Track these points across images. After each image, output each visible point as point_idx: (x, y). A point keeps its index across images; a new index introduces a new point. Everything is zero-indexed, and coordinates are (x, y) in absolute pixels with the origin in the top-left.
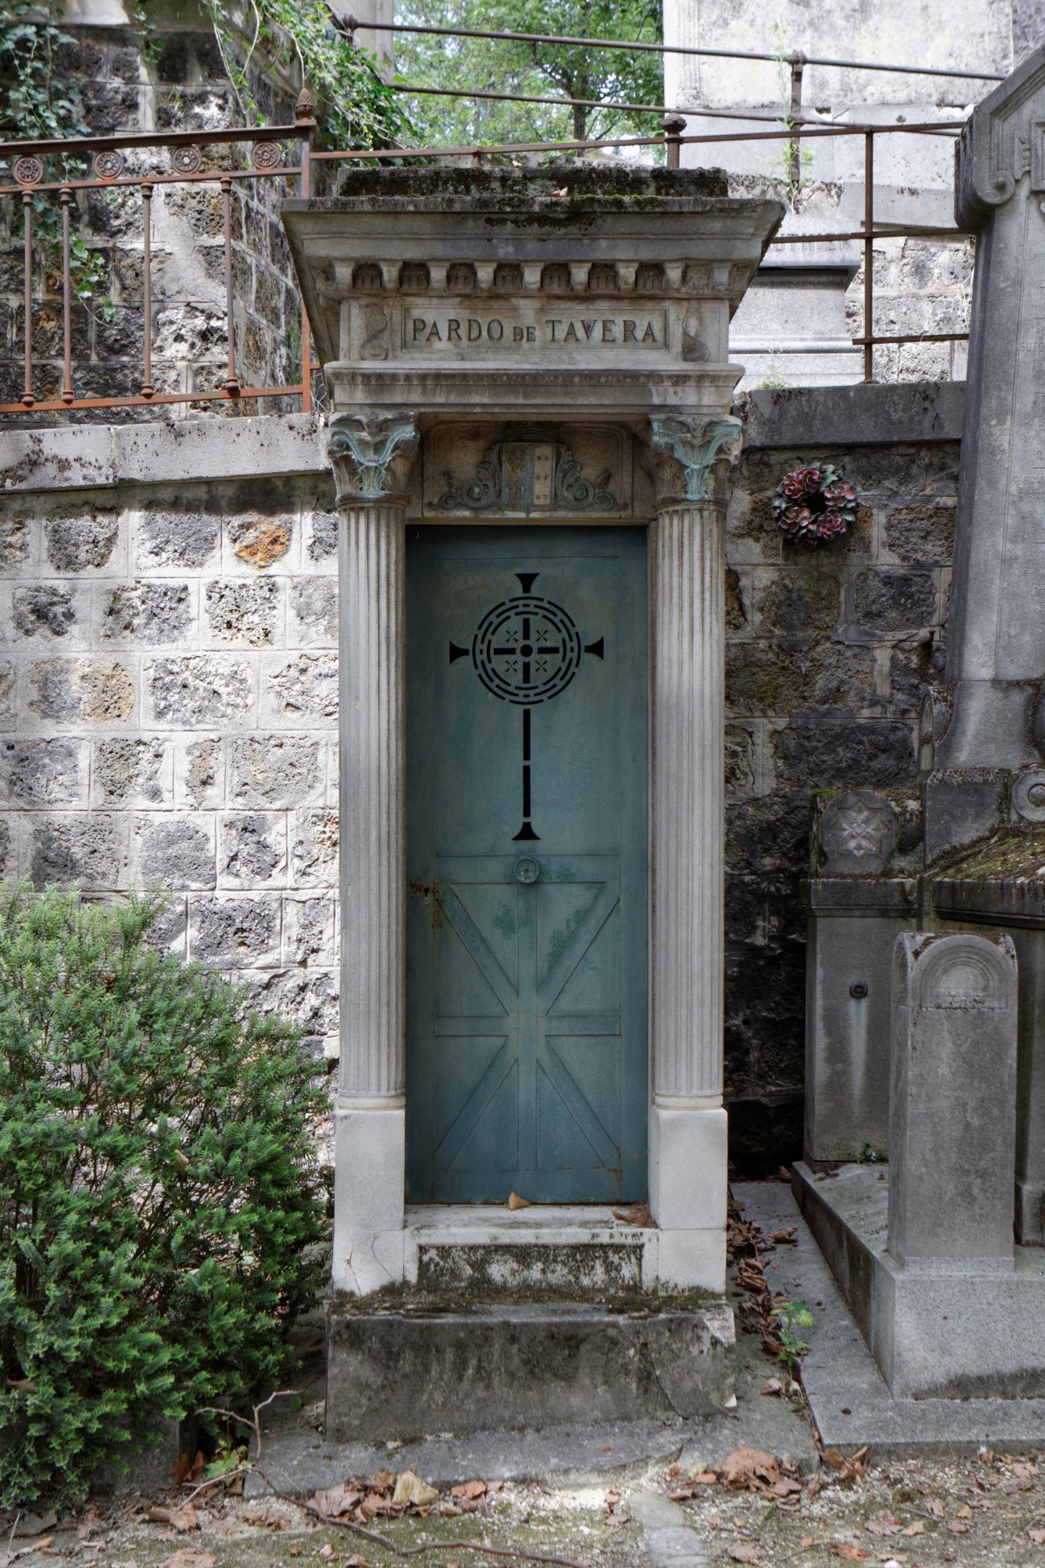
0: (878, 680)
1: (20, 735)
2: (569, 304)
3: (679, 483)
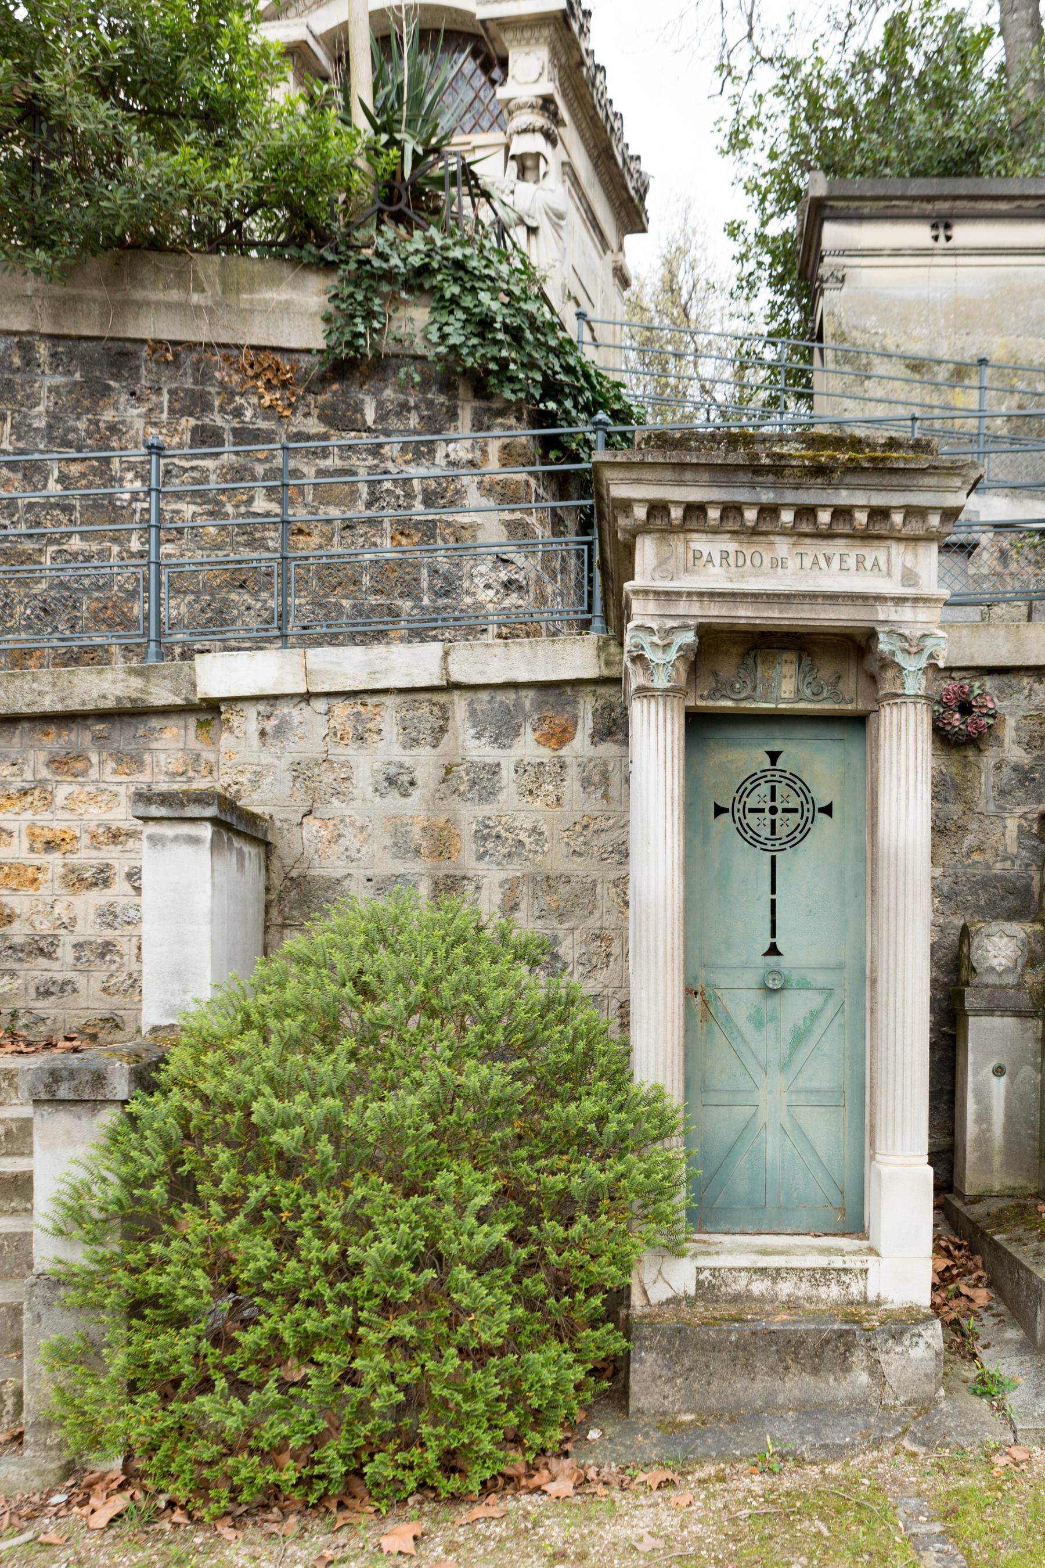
1: (377, 871)
2: (814, 541)
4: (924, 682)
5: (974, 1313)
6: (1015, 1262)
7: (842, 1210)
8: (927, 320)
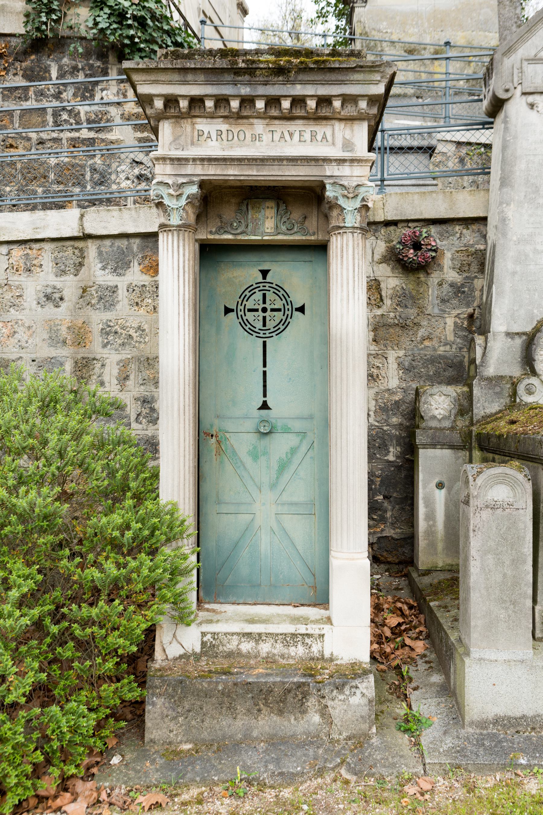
0: (448, 333)
1: (38, 355)
2: (281, 122)
3: (341, 218)
4: (359, 218)
5: (413, 659)
6: (440, 625)
7: (314, 587)
8: (417, 24)
